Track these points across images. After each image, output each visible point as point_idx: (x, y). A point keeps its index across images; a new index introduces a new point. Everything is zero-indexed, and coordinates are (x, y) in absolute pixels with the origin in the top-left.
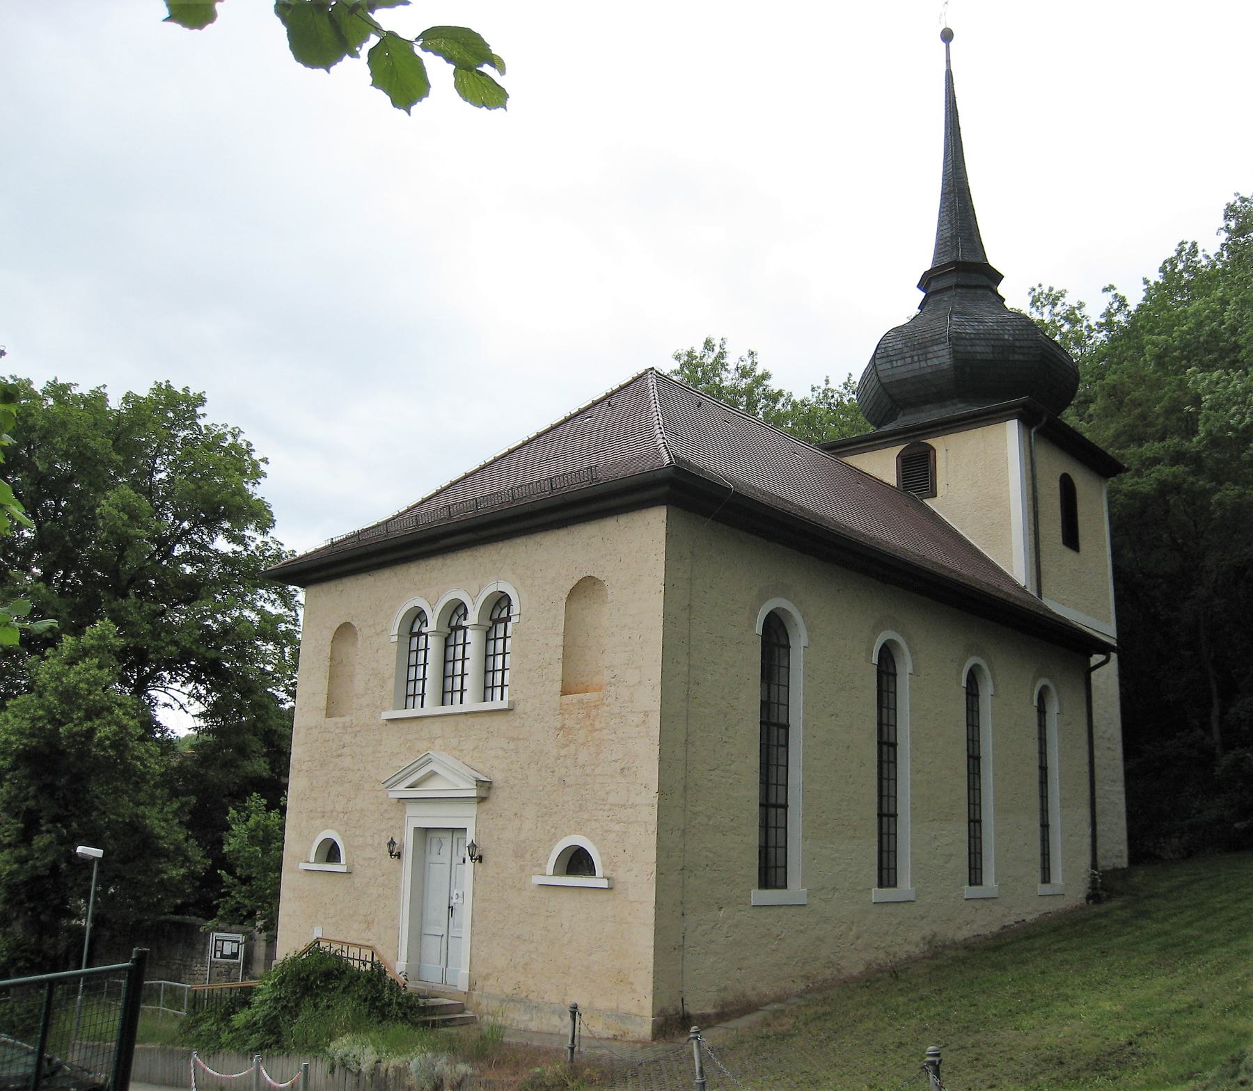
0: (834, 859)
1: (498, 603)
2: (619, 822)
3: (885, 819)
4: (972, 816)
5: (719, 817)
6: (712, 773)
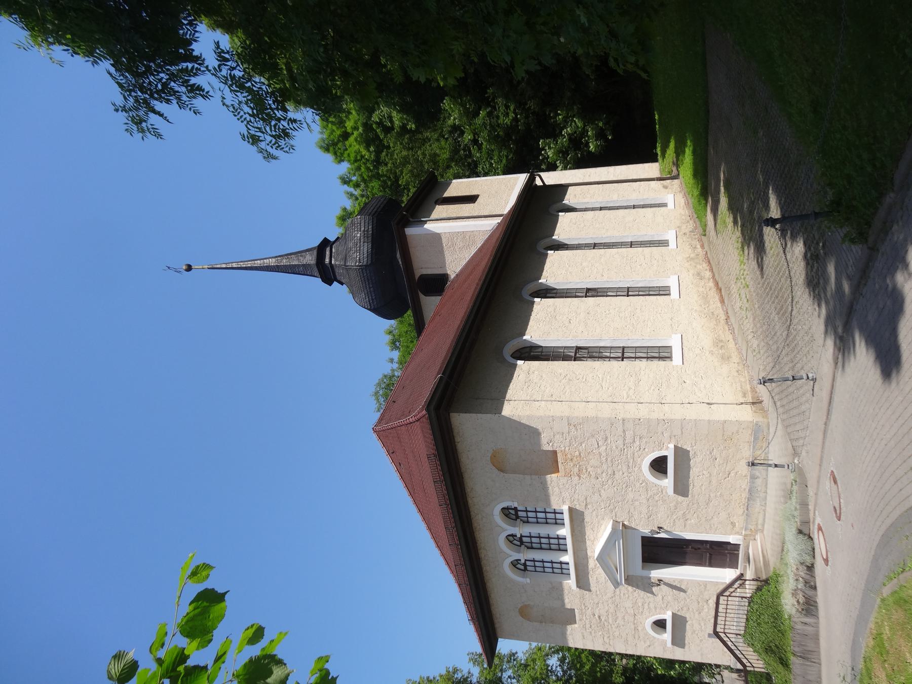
0: (654, 320)
1: (506, 515)
2: (634, 441)
3: (630, 293)
4: (629, 246)
5: (630, 383)
6: (604, 388)
